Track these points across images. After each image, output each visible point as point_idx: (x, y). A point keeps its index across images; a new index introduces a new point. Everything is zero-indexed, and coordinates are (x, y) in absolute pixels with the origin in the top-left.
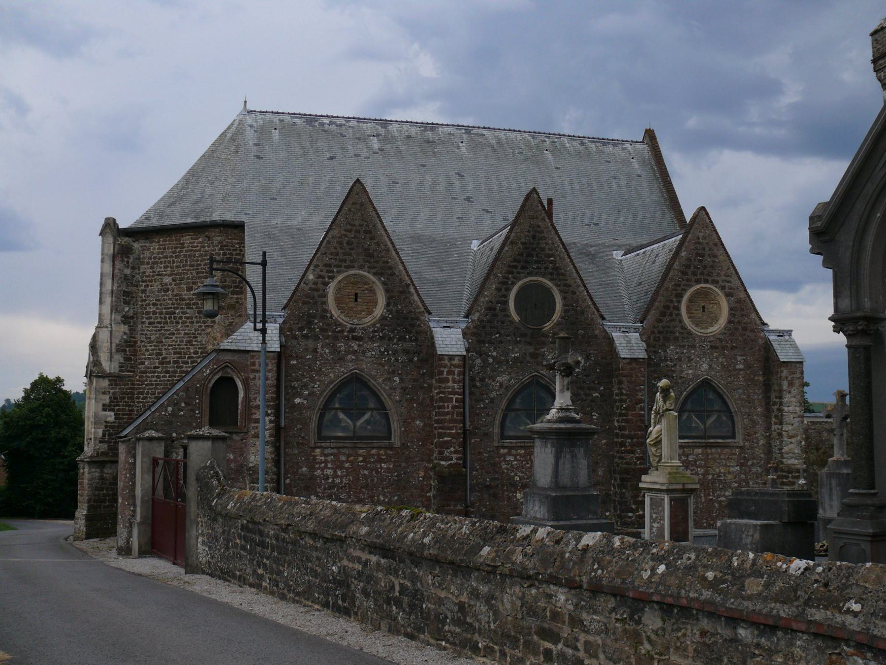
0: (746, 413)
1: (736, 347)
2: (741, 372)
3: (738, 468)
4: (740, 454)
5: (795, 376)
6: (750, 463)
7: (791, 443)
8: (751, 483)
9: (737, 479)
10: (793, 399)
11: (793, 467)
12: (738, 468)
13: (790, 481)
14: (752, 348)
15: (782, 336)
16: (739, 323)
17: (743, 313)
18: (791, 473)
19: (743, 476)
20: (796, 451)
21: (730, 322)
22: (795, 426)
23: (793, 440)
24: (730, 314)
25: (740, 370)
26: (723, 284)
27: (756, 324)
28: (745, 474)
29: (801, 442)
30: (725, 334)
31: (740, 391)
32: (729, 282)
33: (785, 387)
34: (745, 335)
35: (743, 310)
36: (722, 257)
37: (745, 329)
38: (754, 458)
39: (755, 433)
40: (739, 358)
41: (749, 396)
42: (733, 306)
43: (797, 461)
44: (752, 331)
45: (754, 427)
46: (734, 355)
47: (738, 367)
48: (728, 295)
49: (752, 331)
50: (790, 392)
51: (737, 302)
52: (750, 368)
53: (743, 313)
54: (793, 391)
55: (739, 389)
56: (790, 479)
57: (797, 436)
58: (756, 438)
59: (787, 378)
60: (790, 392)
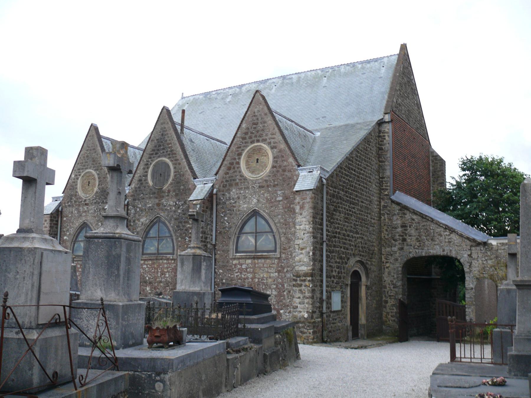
0: (283, 233)
1: (277, 185)
2: (281, 203)
3: (277, 274)
4: (278, 264)
5: (305, 201)
6: (285, 270)
7: (302, 253)
8: (285, 286)
9: (275, 282)
10: (304, 219)
11: (300, 273)
12: (277, 274)
13: (298, 284)
14: (289, 184)
15: (312, 172)
16: (280, 167)
17: (283, 159)
18: (299, 277)
19: (280, 280)
20: (305, 260)
21: (273, 167)
22: (304, 240)
23: (303, 251)
24: (274, 161)
25: (279, 201)
26: (270, 141)
27: (292, 166)
28: (282, 278)
29: (309, 253)
30: (270, 176)
31: (280, 217)
32: (273, 138)
33: (297, 211)
34: (284, 175)
35: (283, 157)
36: (270, 122)
37: (284, 171)
38: (288, 267)
39: (290, 247)
40: (279, 193)
41: (285, 220)
42: (275, 155)
43: (306, 268)
44: (290, 171)
45: (289, 243)
46: (276, 190)
47: (278, 199)
48: (272, 148)
49: (290, 171)
50: (301, 214)
51: (279, 152)
52: (287, 199)
53: (283, 159)
54: (304, 213)
55: (279, 215)
56: (299, 282)
57: (306, 248)
58: (290, 251)
59: (299, 203)
60: (301, 214)
